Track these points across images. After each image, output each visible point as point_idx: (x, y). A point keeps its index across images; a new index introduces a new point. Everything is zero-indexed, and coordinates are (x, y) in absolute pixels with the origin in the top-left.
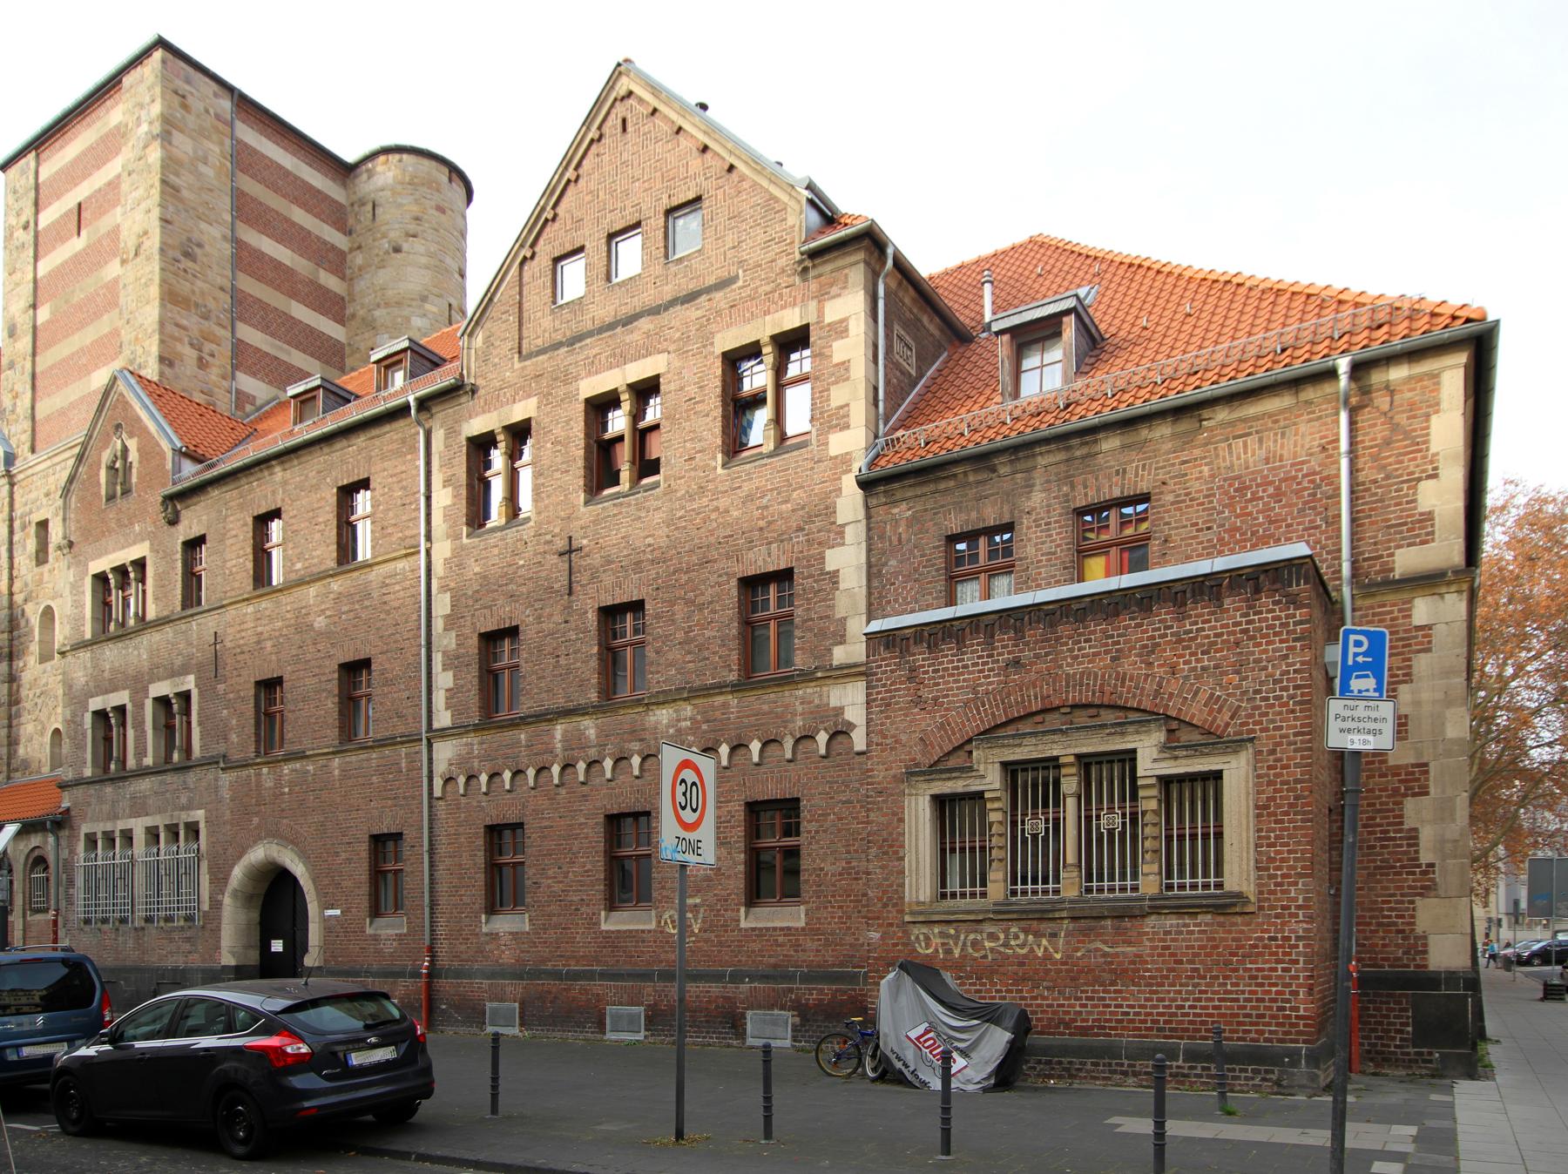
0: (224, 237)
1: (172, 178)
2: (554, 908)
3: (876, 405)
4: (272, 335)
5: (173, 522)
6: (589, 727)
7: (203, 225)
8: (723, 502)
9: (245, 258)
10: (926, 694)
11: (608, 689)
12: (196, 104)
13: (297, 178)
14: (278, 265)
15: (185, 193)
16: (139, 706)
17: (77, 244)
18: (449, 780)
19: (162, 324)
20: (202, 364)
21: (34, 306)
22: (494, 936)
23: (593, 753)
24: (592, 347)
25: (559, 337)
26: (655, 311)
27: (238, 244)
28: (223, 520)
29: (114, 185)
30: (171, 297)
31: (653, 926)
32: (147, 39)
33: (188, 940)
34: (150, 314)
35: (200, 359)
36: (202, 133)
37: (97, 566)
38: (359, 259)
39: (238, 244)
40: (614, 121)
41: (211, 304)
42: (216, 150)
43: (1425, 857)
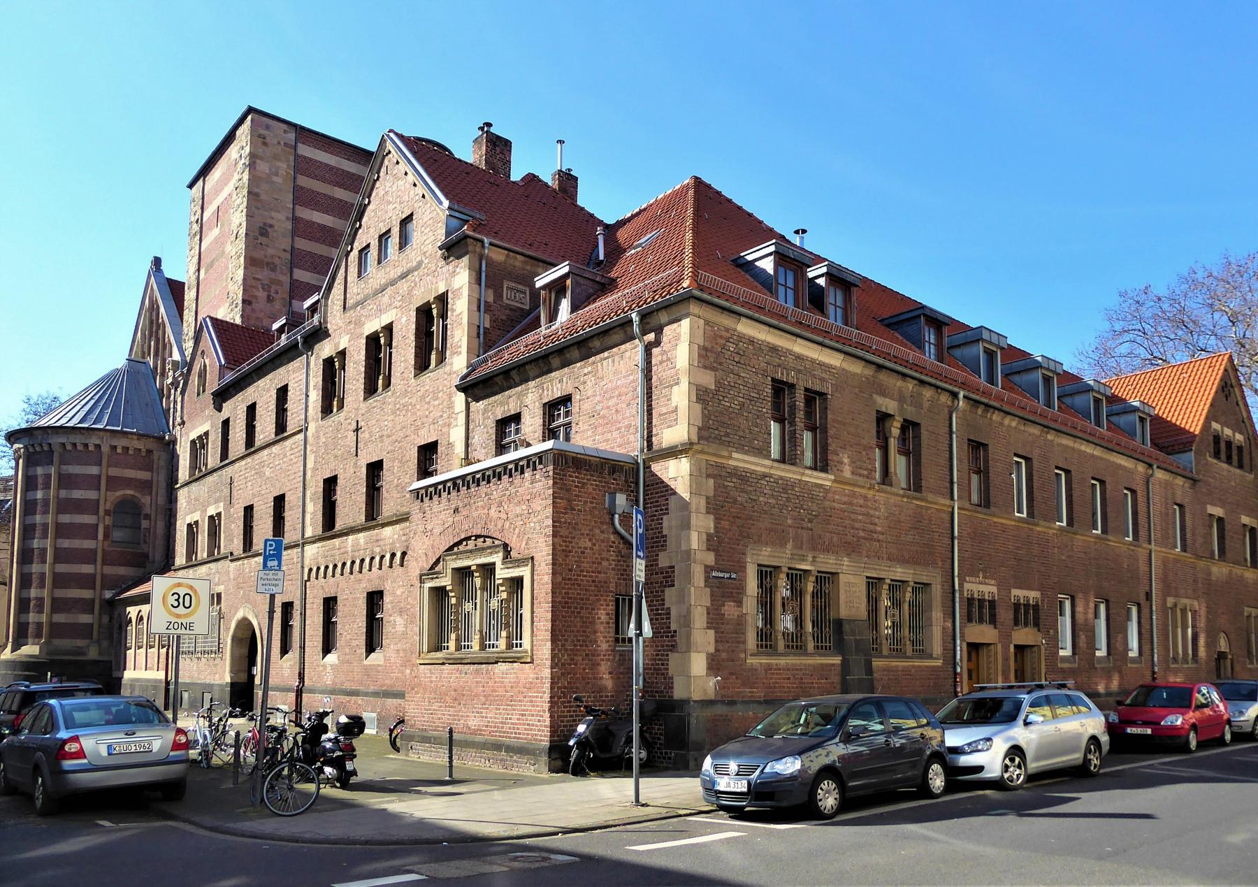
0: (287, 218)
1: (256, 190)
2: (347, 650)
3: (478, 336)
5: (219, 409)
6: (362, 537)
7: (273, 214)
8: (413, 401)
10: (429, 528)
12: (272, 140)
13: (338, 169)
14: (323, 228)
15: (263, 197)
16: (203, 521)
18: (311, 570)
19: (244, 279)
20: (270, 299)
21: (199, 270)
22: (325, 666)
24: (371, 306)
26: (393, 283)
28: (235, 408)
30: (252, 262)
32: (244, 109)
34: (241, 272)
35: (269, 296)
36: (276, 157)
39: (295, 220)
40: (383, 170)
41: (277, 261)
42: (285, 167)
43: (673, 627)
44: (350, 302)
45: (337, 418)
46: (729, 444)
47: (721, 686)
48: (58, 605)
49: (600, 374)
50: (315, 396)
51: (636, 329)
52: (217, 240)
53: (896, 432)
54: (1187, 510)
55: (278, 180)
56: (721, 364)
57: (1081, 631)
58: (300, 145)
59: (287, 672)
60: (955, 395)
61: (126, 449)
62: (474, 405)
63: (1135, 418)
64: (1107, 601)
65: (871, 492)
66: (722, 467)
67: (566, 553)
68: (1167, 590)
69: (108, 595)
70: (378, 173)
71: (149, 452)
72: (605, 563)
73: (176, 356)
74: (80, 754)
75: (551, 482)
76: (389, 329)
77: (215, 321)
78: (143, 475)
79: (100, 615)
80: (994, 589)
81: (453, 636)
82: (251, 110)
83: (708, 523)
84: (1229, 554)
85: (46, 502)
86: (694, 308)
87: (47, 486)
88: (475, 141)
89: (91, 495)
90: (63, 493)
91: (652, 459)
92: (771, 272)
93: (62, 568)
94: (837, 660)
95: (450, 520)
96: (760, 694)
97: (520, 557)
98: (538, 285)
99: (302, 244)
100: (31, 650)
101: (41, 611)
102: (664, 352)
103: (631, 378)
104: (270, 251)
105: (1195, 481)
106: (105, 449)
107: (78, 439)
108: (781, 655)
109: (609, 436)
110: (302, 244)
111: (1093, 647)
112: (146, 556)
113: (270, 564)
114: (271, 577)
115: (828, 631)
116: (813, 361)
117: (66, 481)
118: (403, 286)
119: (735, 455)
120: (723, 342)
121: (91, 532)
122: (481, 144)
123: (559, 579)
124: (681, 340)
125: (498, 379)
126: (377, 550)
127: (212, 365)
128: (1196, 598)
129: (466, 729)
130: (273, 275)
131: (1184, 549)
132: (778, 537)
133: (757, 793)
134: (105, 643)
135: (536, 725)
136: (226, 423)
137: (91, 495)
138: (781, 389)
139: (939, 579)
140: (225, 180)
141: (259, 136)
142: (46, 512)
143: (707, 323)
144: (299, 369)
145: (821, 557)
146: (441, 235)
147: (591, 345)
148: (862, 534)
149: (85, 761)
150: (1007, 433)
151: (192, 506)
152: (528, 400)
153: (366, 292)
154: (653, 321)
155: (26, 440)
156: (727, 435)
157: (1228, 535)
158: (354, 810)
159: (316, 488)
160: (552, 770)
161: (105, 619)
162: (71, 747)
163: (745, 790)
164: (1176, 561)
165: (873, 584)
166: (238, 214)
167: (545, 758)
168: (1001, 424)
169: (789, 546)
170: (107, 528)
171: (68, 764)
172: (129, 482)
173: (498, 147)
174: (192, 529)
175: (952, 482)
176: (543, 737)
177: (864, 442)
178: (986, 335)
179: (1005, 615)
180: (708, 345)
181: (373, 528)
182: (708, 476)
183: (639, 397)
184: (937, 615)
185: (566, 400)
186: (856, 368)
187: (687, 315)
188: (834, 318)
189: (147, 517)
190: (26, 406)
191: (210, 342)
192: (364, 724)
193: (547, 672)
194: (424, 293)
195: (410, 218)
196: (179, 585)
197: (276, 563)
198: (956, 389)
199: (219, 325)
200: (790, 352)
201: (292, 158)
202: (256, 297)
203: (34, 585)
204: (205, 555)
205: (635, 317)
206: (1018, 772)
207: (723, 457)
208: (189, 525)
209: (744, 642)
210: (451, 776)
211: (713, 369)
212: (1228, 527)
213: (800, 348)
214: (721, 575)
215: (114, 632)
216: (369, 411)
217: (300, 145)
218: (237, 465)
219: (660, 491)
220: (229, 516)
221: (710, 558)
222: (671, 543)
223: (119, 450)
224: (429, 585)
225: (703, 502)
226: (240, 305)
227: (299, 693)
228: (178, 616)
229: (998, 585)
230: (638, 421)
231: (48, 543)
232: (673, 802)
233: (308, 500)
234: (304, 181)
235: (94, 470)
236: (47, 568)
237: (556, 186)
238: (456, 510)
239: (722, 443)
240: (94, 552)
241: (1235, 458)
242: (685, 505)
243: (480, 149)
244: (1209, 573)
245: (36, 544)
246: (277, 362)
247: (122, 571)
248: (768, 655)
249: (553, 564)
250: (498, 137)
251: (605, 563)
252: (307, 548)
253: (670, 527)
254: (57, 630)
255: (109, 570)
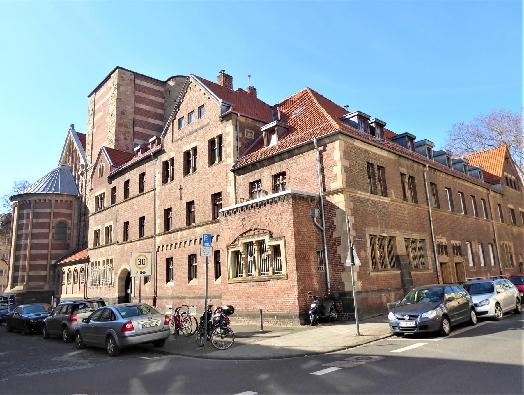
0: (132, 108)
1: (120, 97)
2: (179, 280)
4: (144, 128)
5: (111, 183)
6: (185, 232)
7: (127, 106)
8: (208, 176)
9: (137, 111)
10: (230, 227)
11: (189, 223)
14: (145, 111)
15: (122, 100)
16: (103, 229)
17: (101, 114)
18: (159, 247)
19: (116, 132)
20: (125, 139)
22: (167, 287)
23: (185, 239)
24: (185, 140)
25: (179, 137)
26: (196, 131)
27: (135, 108)
28: (119, 183)
29: (108, 100)
30: (118, 125)
31: (197, 284)
32: (115, 67)
33: (110, 290)
34: (114, 130)
35: (125, 138)
36: (127, 85)
37: (96, 195)
38: (166, 104)
39: (135, 108)
40: (189, 89)
41: (128, 124)
42: (130, 88)
44: (175, 139)
45: (169, 185)
46: (355, 188)
47: (363, 285)
48: (32, 268)
49: (298, 163)
50: (159, 177)
51: (315, 145)
52: (102, 117)
53: (407, 181)
54: (502, 206)
55: (128, 93)
56: (350, 157)
57: (474, 255)
58: (136, 80)
59: (148, 291)
60: (425, 166)
61: (61, 201)
62: (238, 177)
63: (477, 172)
64: (482, 244)
65: (402, 204)
66: (354, 197)
67: (299, 234)
68: (500, 238)
69: (53, 262)
70: (187, 90)
71: (71, 202)
72: (312, 237)
73: (82, 162)
74: (132, 329)
75: (291, 206)
76: (195, 149)
77: (106, 148)
78: (68, 211)
79: (50, 271)
80: (445, 241)
81: (244, 271)
82: (118, 67)
83: (352, 219)
84: (517, 223)
85: (27, 224)
86: (340, 137)
87: (28, 218)
88: (219, 77)
89: (47, 220)
90: (35, 221)
91: (326, 195)
92: (357, 122)
93: (34, 252)
94: (399, 272)
95: (241, 223)
96: (375, 287)
97: (278, 236)
98: (262, 130)
99: (138, 117)
100: (19, 288)
101: (24, 271)
102: (328, 154)
103: (313, 164)
104: (126, 120)
105: (503, 195)
106: (53, 201)
107: (42, 198)
108: (381, 271)
109: (305, 187)
110: (138, 117)
111: (480, 263)
112: (69, 245)
113: (205, 244)
114: (206, 249)
115: (394, 260)
116: (379, 155)
117: (36, 215)
118: (201, 132)
119: (359, 192)
120: (350, 149)
121: (46, 236)
122: (221, 78)
123: (297, 245)
124: (336, 149)
125: (250, 167)
126: (193, 237)
127: (107, 165)
128: (509, 241)
129: (268, 309)
130: (127, 130)
131: (503, 222)
132: (375, 224)
133: (420, 327)
134: (52, 283)
135: (293, 306)
136: (114, 189)
137: (47, 220)
138: (370, 165)
139: (428, 237)
140: (106, 93)
141: (121, 77)
142: (27, 228)
143: (345, 142)
144: (150, 166)
145: (390, 231)
146: (219, 112)
147: (293, 152)
148: (401, 221)
149: (134, 331)
150: (443, 180)
151: (96, 223)
152: (265, 175)
153: (182, 135)
154: (322, 142)
155: (19, 199)
156: (355, 184)
157: (516, 215)
158: (242, 346)
159: (161, 213)
160: (302, 324)
161: (52, 273)
162: (129, 326)
163: (415, 325)
164: (502, 226)
165: (407, 240)
166: (112, 107)
167: (298, 320)
168: (440, 176)
169: (379, 227)
170: (53, 234)
171: (127, 333)
172: (62, 215)
173: (228, 79)
174: (97, 234)
175: (427, 199)
176: (296, 310)
177: (398, 185)
178: (427, 143)
179: (450, 251)
180: (346, 150)
181: (191, 228)
182: (350, 201)
183: (323, 171)
184: (429, 252)
185: (283, 174)
186: (392, 157)
187: (338, 139)
188: (378, 138)
189: (70, 229)
190: (14, 185)
191: (105, 156)
192: (234, 309)
193: (295, 283)
194: (213, 134)
195: (203, 106)
196: (141, 255)
197: (208, 244)
198: (425, 163)
199: (108, 150)
200: (371, 151)
201: (133, 85)
202: (120, 138)
203: (21, 260)
204: (104, 243)
205: (315, 141)
206: (500, 313)
207: (354, 193)
208: (96, 231)
209: (368, 267)
210: (262, 329)
211: (348, 159)
212: (515, 213)
213: (375, 150)
214: (358, 239)
215: (56, 278)
216: (186, 181)
217: (136, 80)
218: (120, 205)
219: (332, 208)
220: (116, 226)
221: (353, 233)
222: (338, 228)
223: (59, 202)
224: (231, 250)
225: (350, 211)
226: (114, 142)
227: (155, 299)
228: (140, 268)
229: (446, 239)
230: (319, 181)
231: (28, 242)
232: (377, 334)
233: (157, 218)
234: (138, 93)
235: (48, 210)
236: (27, 252)
237: (249, 92)
238: (244, 219)
239: (354, 187)
240: (48, 244)
241: (513, 185)
242: (343, 213)
243: (221, 80)
244: (512, 231)
245: (22, 242)
246: (140, 163)
247: (59, 252)
248: (385, 271)
249: (295, 239)
250: (228, 75)
251: (312, 237)
252: (157, 238)
253: (337, 222)
254: (31, 279)
255: (54, 252)
